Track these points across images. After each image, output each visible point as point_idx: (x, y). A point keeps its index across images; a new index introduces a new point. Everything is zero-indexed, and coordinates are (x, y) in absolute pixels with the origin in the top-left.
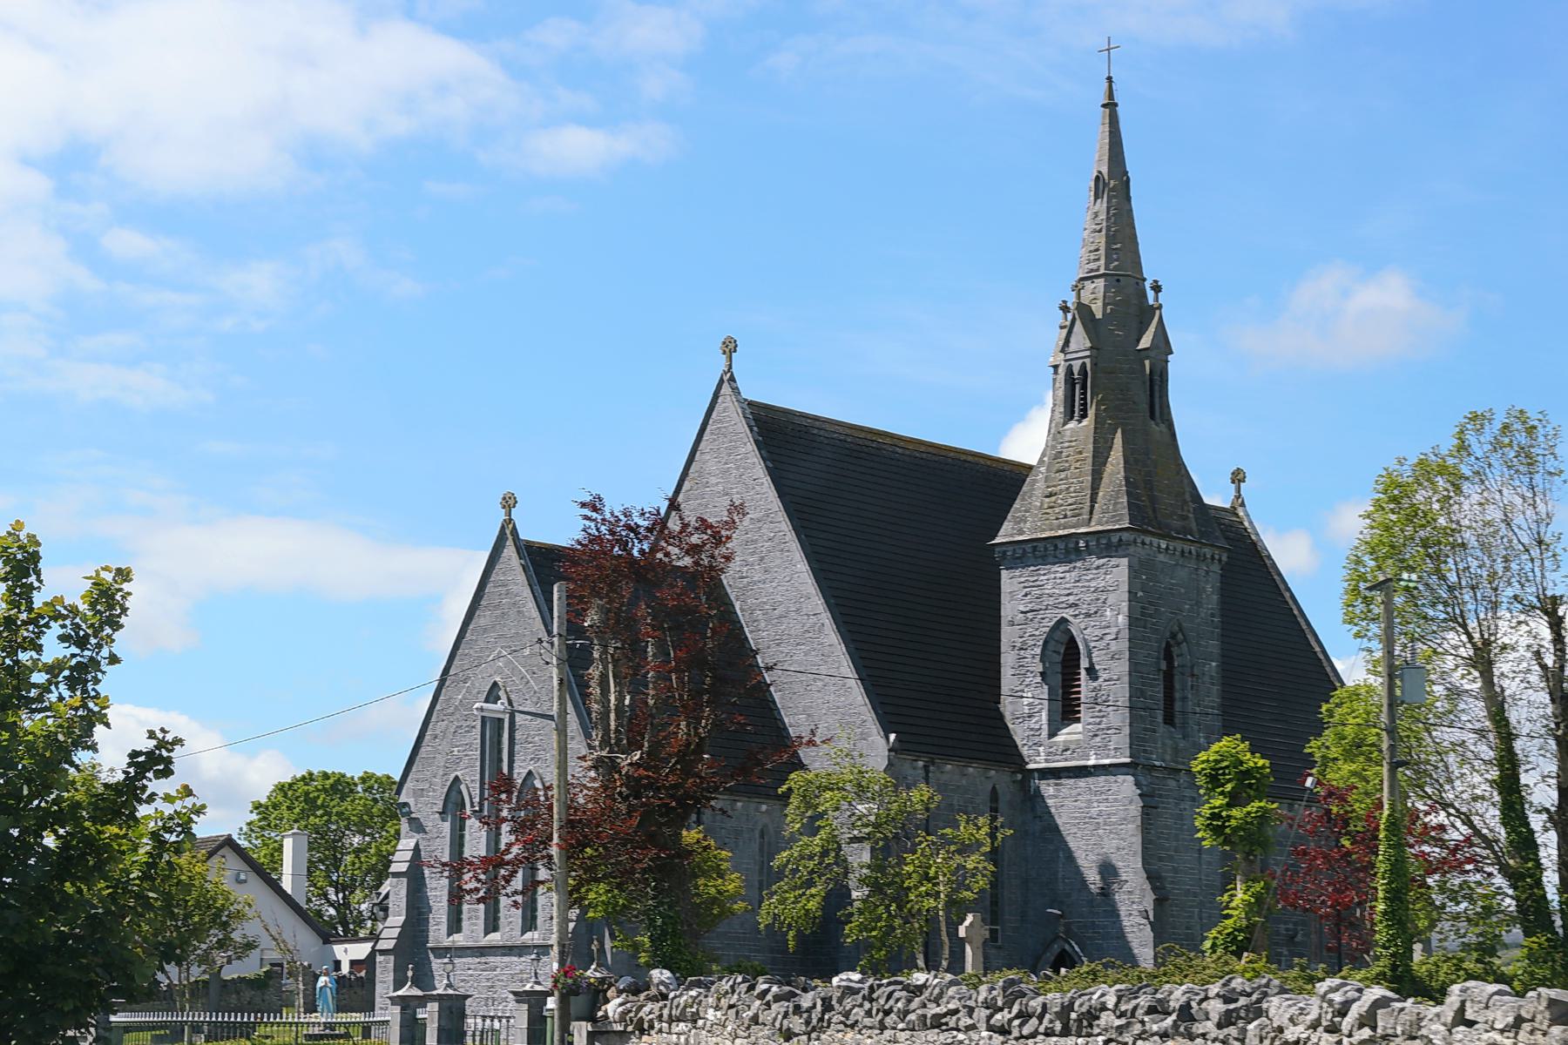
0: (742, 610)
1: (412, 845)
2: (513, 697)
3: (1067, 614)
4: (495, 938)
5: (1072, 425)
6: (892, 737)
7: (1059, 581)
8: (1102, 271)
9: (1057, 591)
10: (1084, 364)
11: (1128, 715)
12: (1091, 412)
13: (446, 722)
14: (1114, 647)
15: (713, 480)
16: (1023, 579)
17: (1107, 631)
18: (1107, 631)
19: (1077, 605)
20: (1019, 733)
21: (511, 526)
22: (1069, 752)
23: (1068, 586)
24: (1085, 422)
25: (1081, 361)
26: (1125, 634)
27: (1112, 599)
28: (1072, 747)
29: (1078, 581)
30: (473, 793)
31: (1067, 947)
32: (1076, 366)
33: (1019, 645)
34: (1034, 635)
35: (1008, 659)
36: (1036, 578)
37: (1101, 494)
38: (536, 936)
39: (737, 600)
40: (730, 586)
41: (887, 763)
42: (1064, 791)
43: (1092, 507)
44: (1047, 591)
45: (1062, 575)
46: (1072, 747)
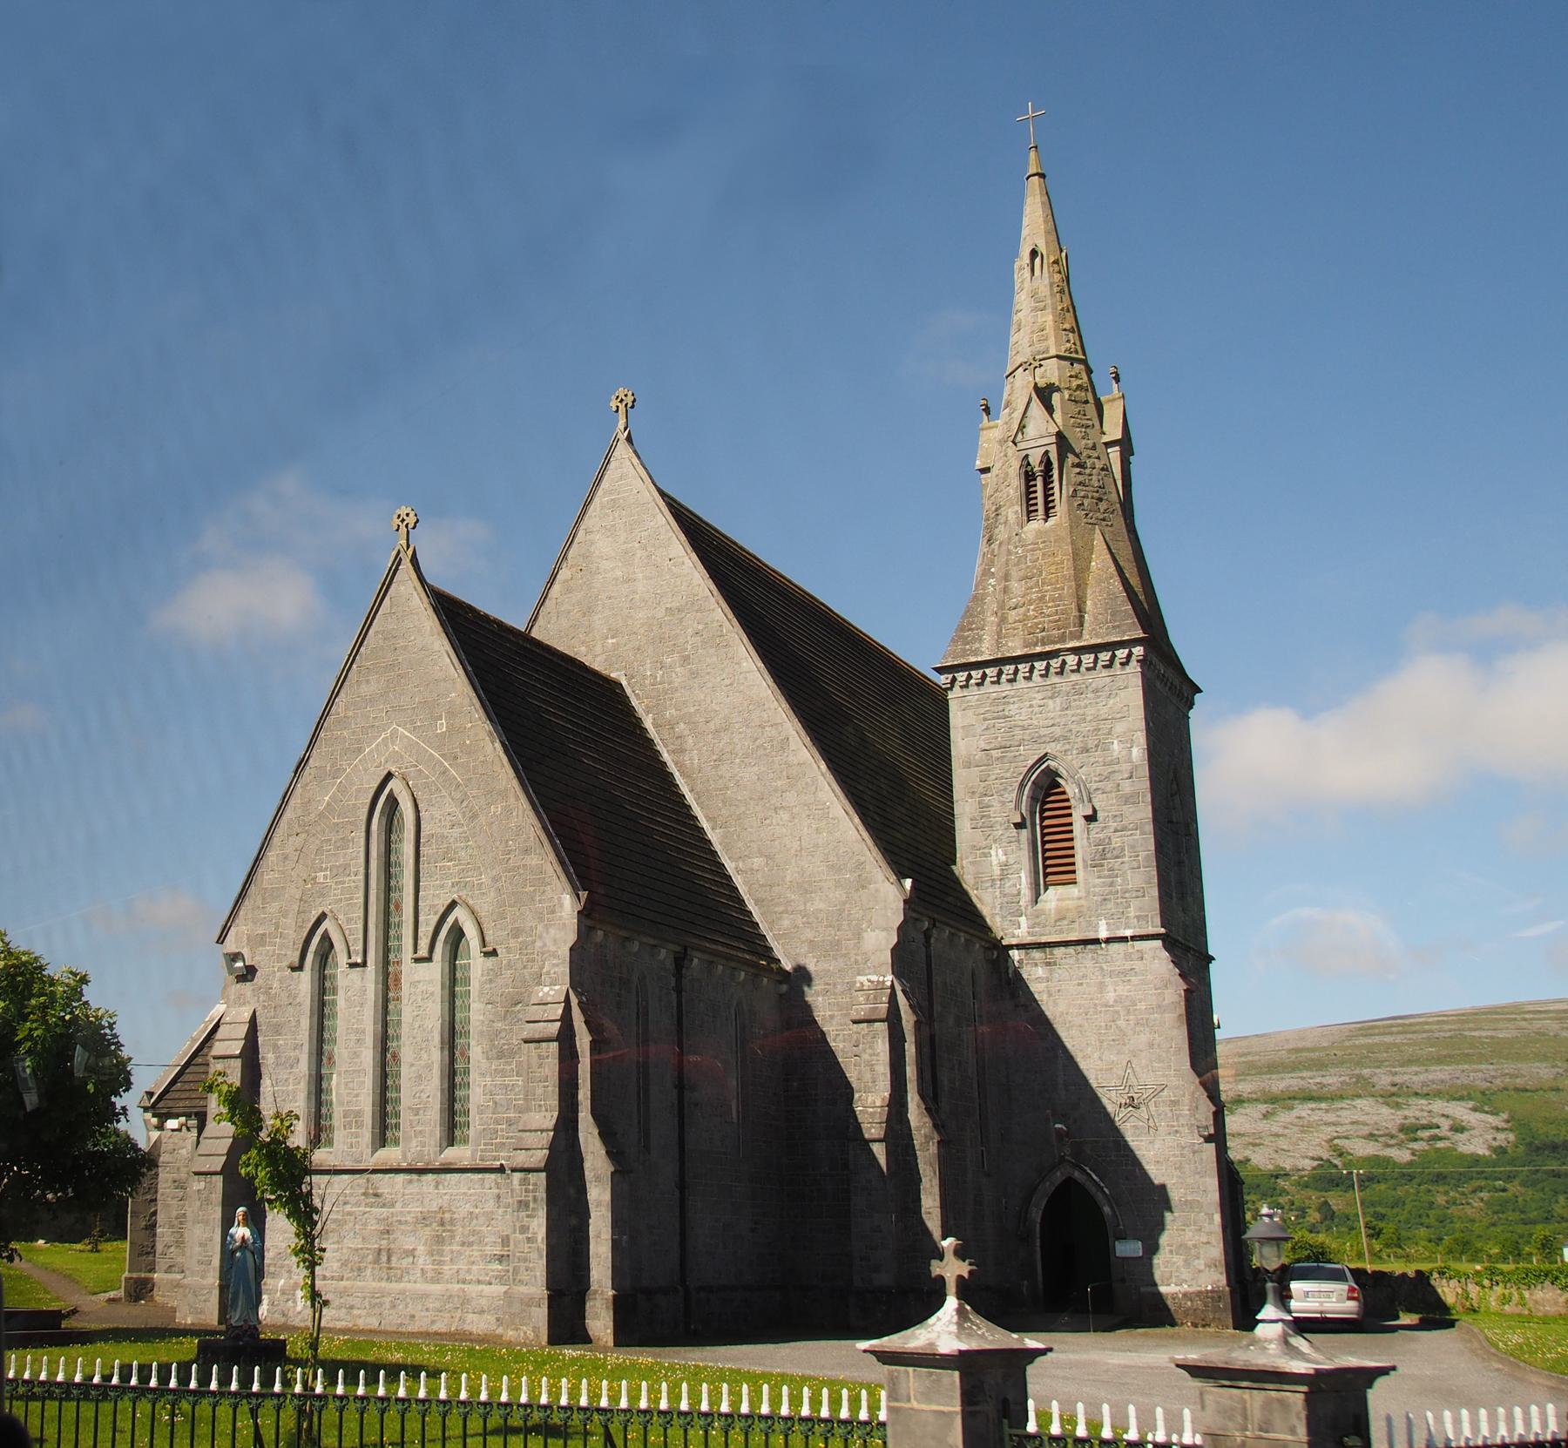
0: (656, 726)
1: (247, 1016)
2: (418, 795)
3: (1051, 748)
4: (454, 1154)
5: (1034, 525)
6: (908, 883)
7: (1037, 709)
8: (1053, 352)
9: (1035, 722)
10: (1046, 452)
11: (1155, 873)
12: (1061, 508)
13: (303, 836)
14: (1127, 787)
15: (606, 565)
16: (982, 711)
17: (1116, 767)
18: (1116, 767)
19: (1066, 738)
20: (987, 903)
21: (410, 552)
22: (1065, 922)
23: (1052, 715)
24: (1052, 521)
25: (1043, 450)
26: (1145, 771)
27: (1119, 728)
28: (1069, 915)
29: (1067, 709)
30: (350, 938)
31: (1077, 1174)
32: (1035, 459)
33: (981, 790)
34: (1002, 778)
35: (964, 810)
36: (1001, 708)
37: (1089, 603)
38: (468, 1154)
39: (648, 713)
40: (637, 695)
41: (902, 919)
42: (1059, 973)
43: (1081, 617)
44: (1020, 723)
45: (1042, 702)
46: (1069, 915)
